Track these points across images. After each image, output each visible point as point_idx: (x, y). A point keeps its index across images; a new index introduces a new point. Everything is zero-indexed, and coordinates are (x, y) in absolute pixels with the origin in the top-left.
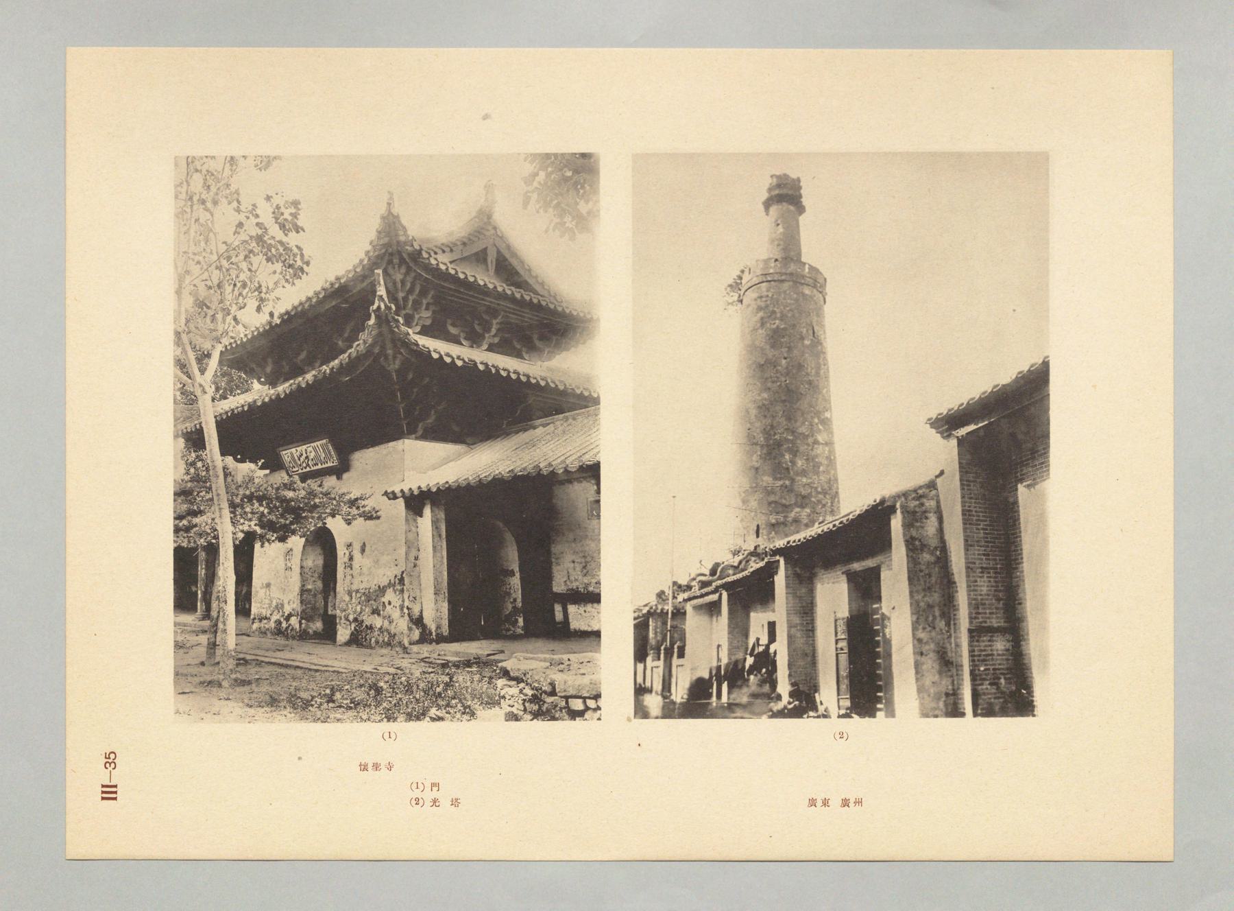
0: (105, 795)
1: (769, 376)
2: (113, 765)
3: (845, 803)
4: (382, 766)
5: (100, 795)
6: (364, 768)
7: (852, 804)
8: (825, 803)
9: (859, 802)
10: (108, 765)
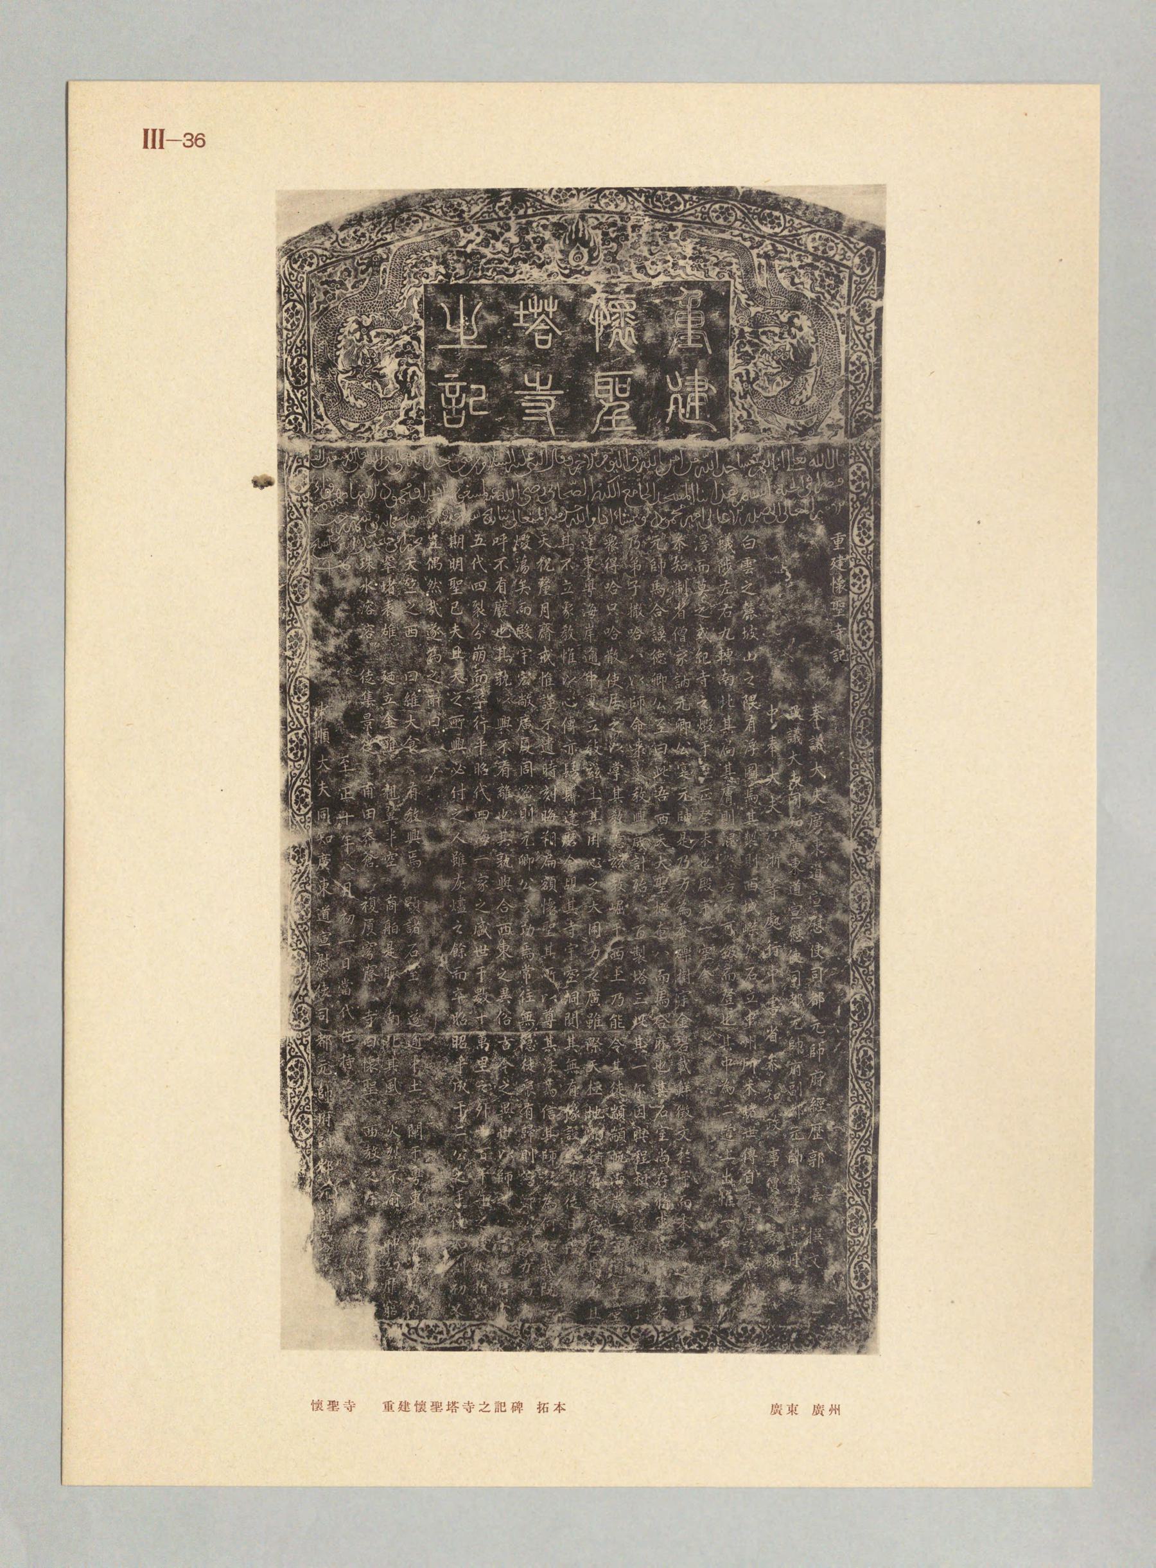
0: (150, 133)
1: (457, 746)
2: (189, 143)
3: (818, 1410)
4: (341, 1406)
5: (150, 127)
6: (388, 1406)
7: (826, 1412)
8: (792, 1410)
9: (835, 1409)
10: (189, 137)
